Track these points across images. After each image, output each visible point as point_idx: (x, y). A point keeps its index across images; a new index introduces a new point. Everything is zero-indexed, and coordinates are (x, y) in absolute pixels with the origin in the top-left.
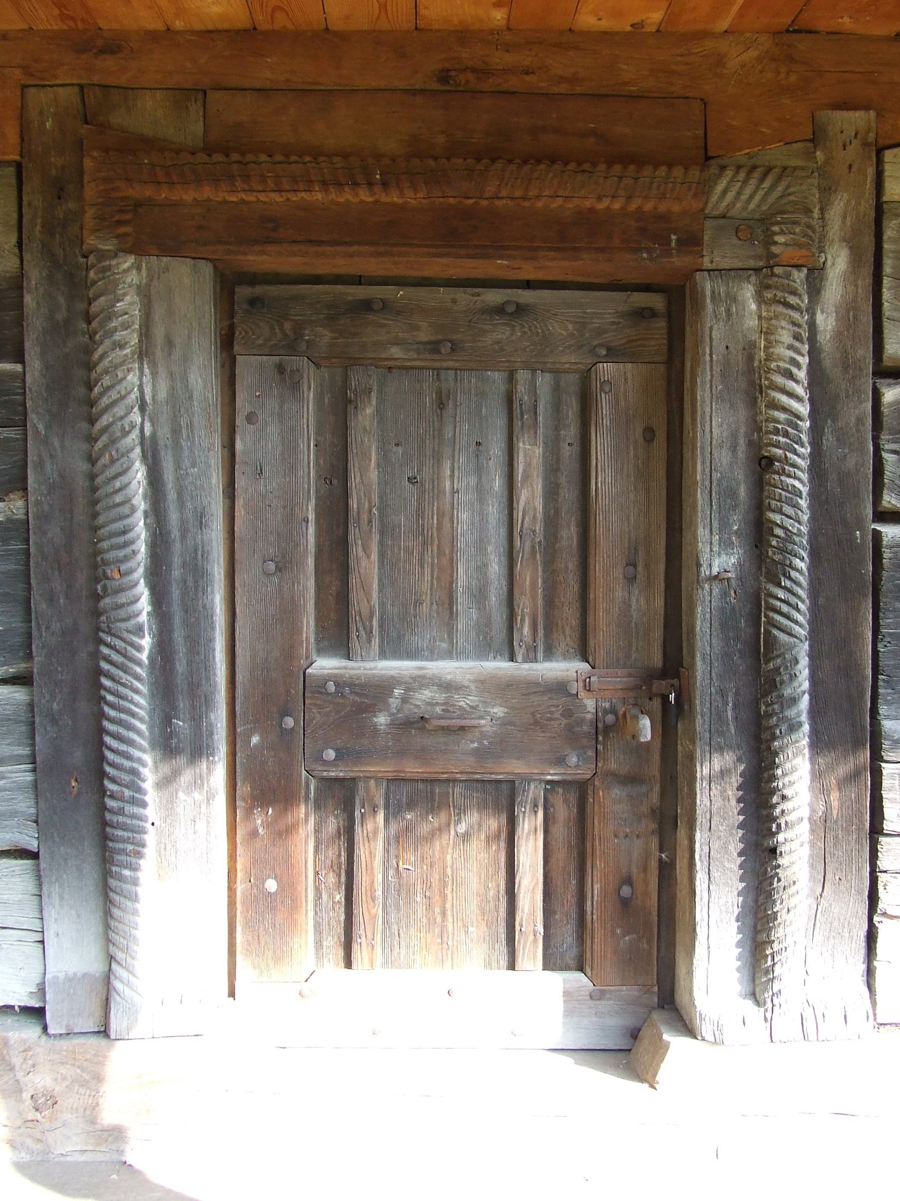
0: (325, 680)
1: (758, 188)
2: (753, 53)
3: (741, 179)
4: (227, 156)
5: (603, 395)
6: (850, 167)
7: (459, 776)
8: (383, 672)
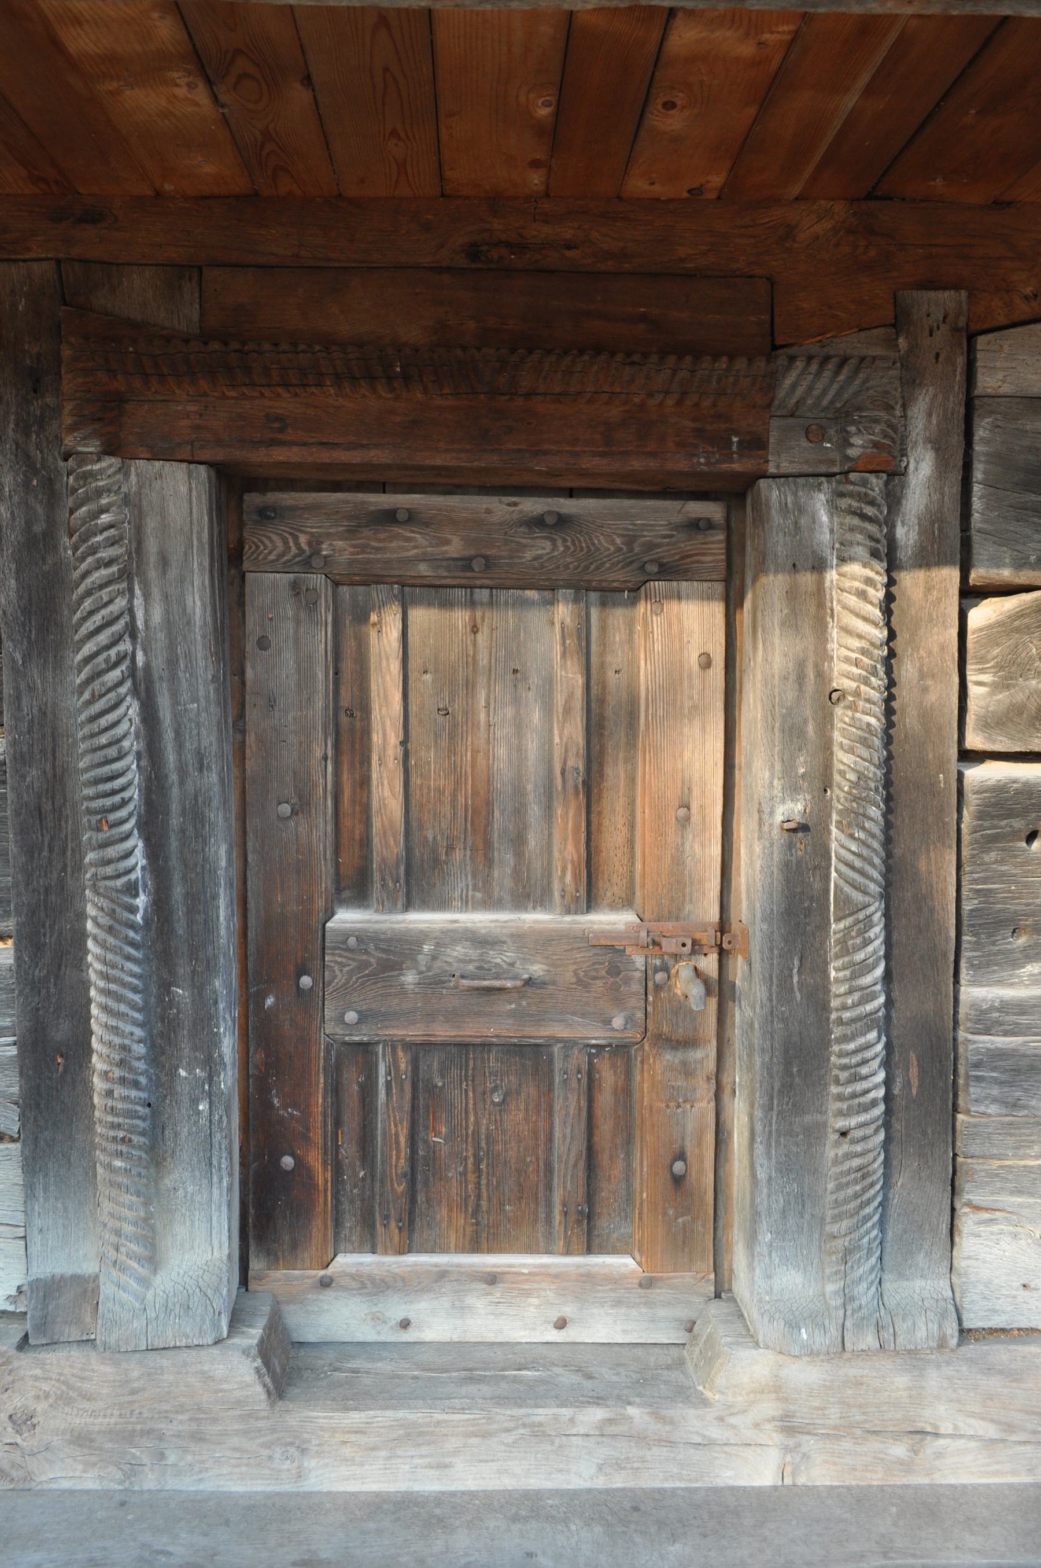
0: (346, 935)
1: (832, 381)
2: (827, 225)
3: (813, 371)
4: (226, 344)
5: (654, 618)
6: (937, 356)
7: (494, 1040)
8: (412, 926)
